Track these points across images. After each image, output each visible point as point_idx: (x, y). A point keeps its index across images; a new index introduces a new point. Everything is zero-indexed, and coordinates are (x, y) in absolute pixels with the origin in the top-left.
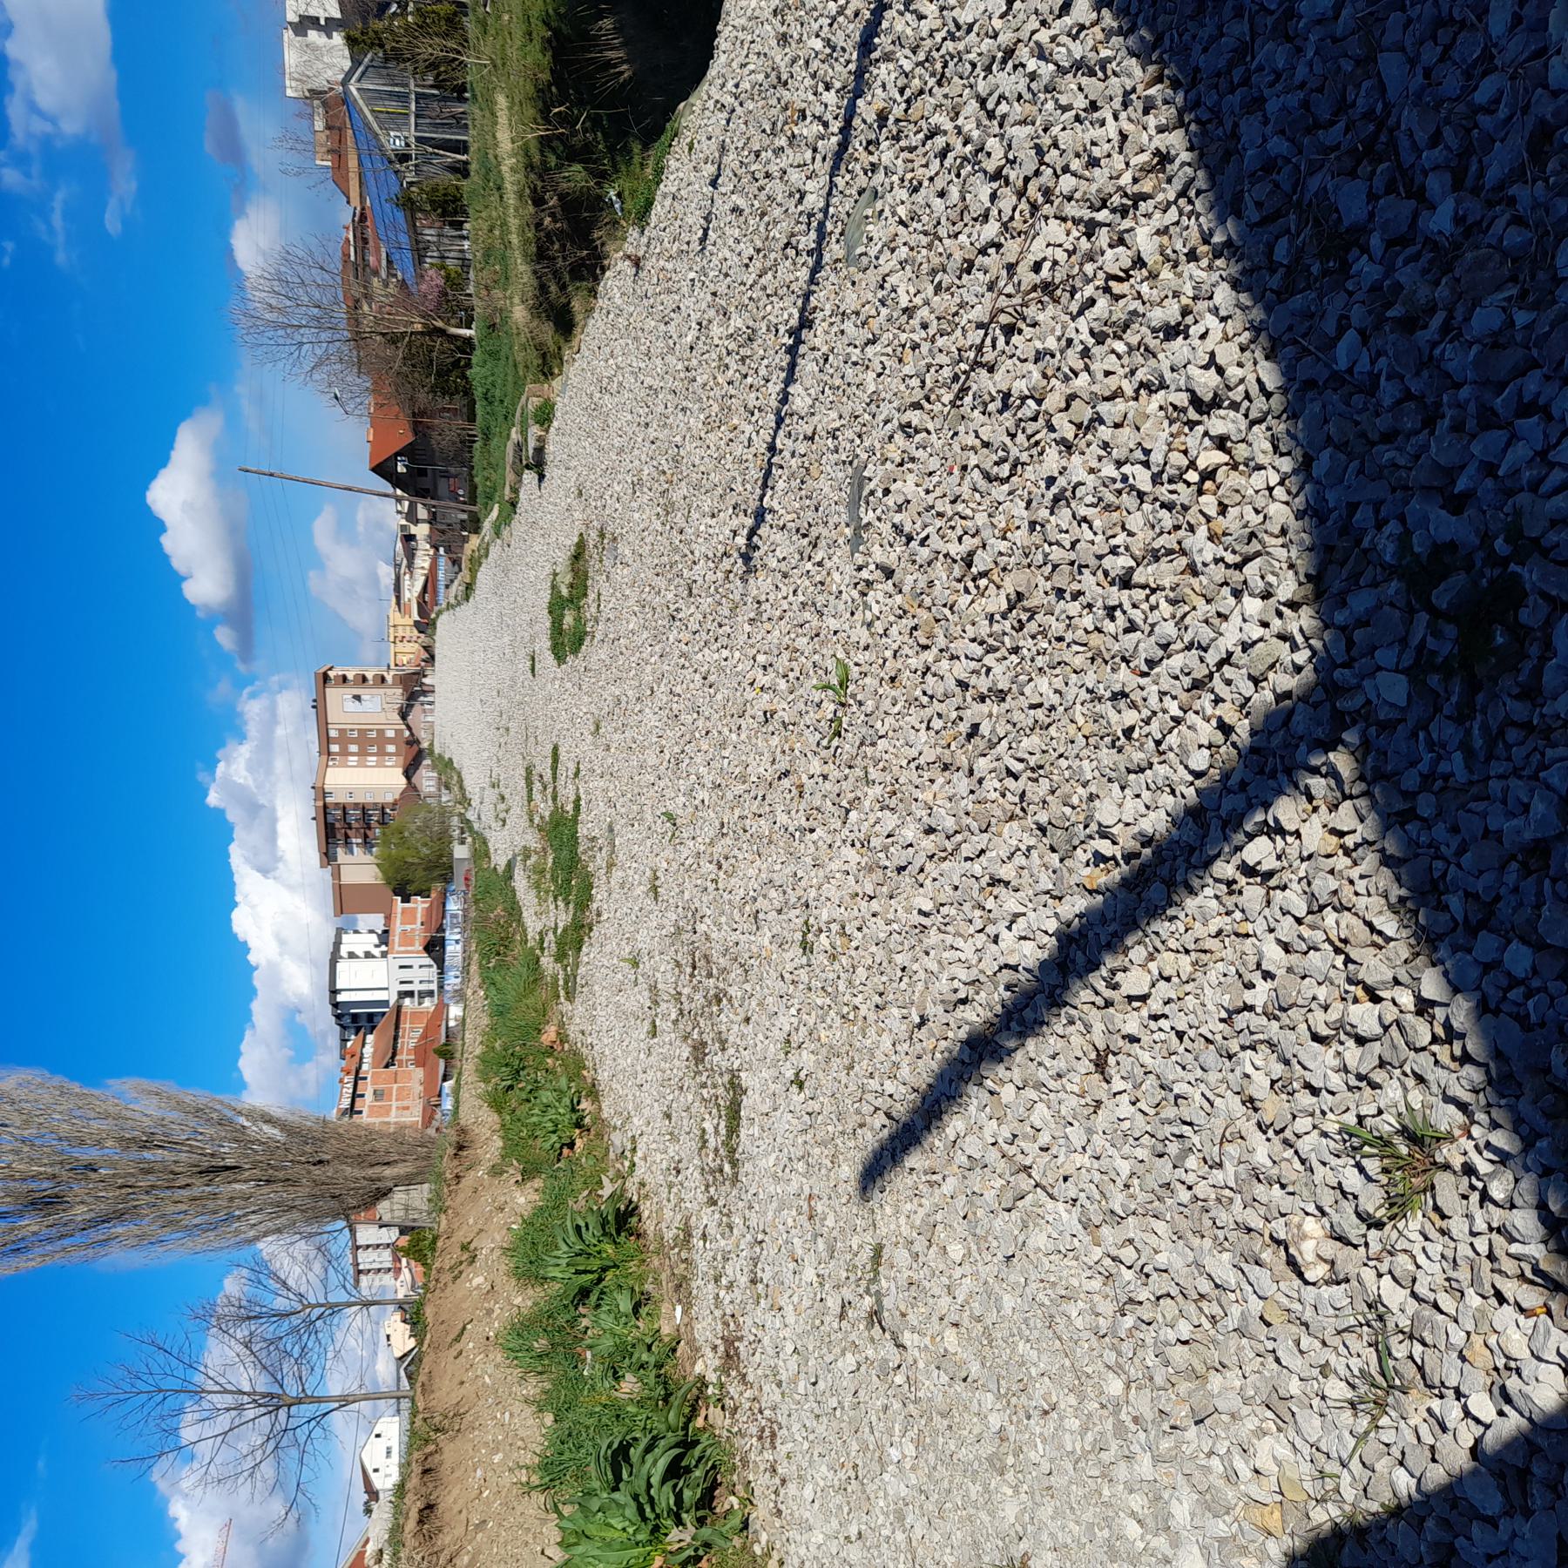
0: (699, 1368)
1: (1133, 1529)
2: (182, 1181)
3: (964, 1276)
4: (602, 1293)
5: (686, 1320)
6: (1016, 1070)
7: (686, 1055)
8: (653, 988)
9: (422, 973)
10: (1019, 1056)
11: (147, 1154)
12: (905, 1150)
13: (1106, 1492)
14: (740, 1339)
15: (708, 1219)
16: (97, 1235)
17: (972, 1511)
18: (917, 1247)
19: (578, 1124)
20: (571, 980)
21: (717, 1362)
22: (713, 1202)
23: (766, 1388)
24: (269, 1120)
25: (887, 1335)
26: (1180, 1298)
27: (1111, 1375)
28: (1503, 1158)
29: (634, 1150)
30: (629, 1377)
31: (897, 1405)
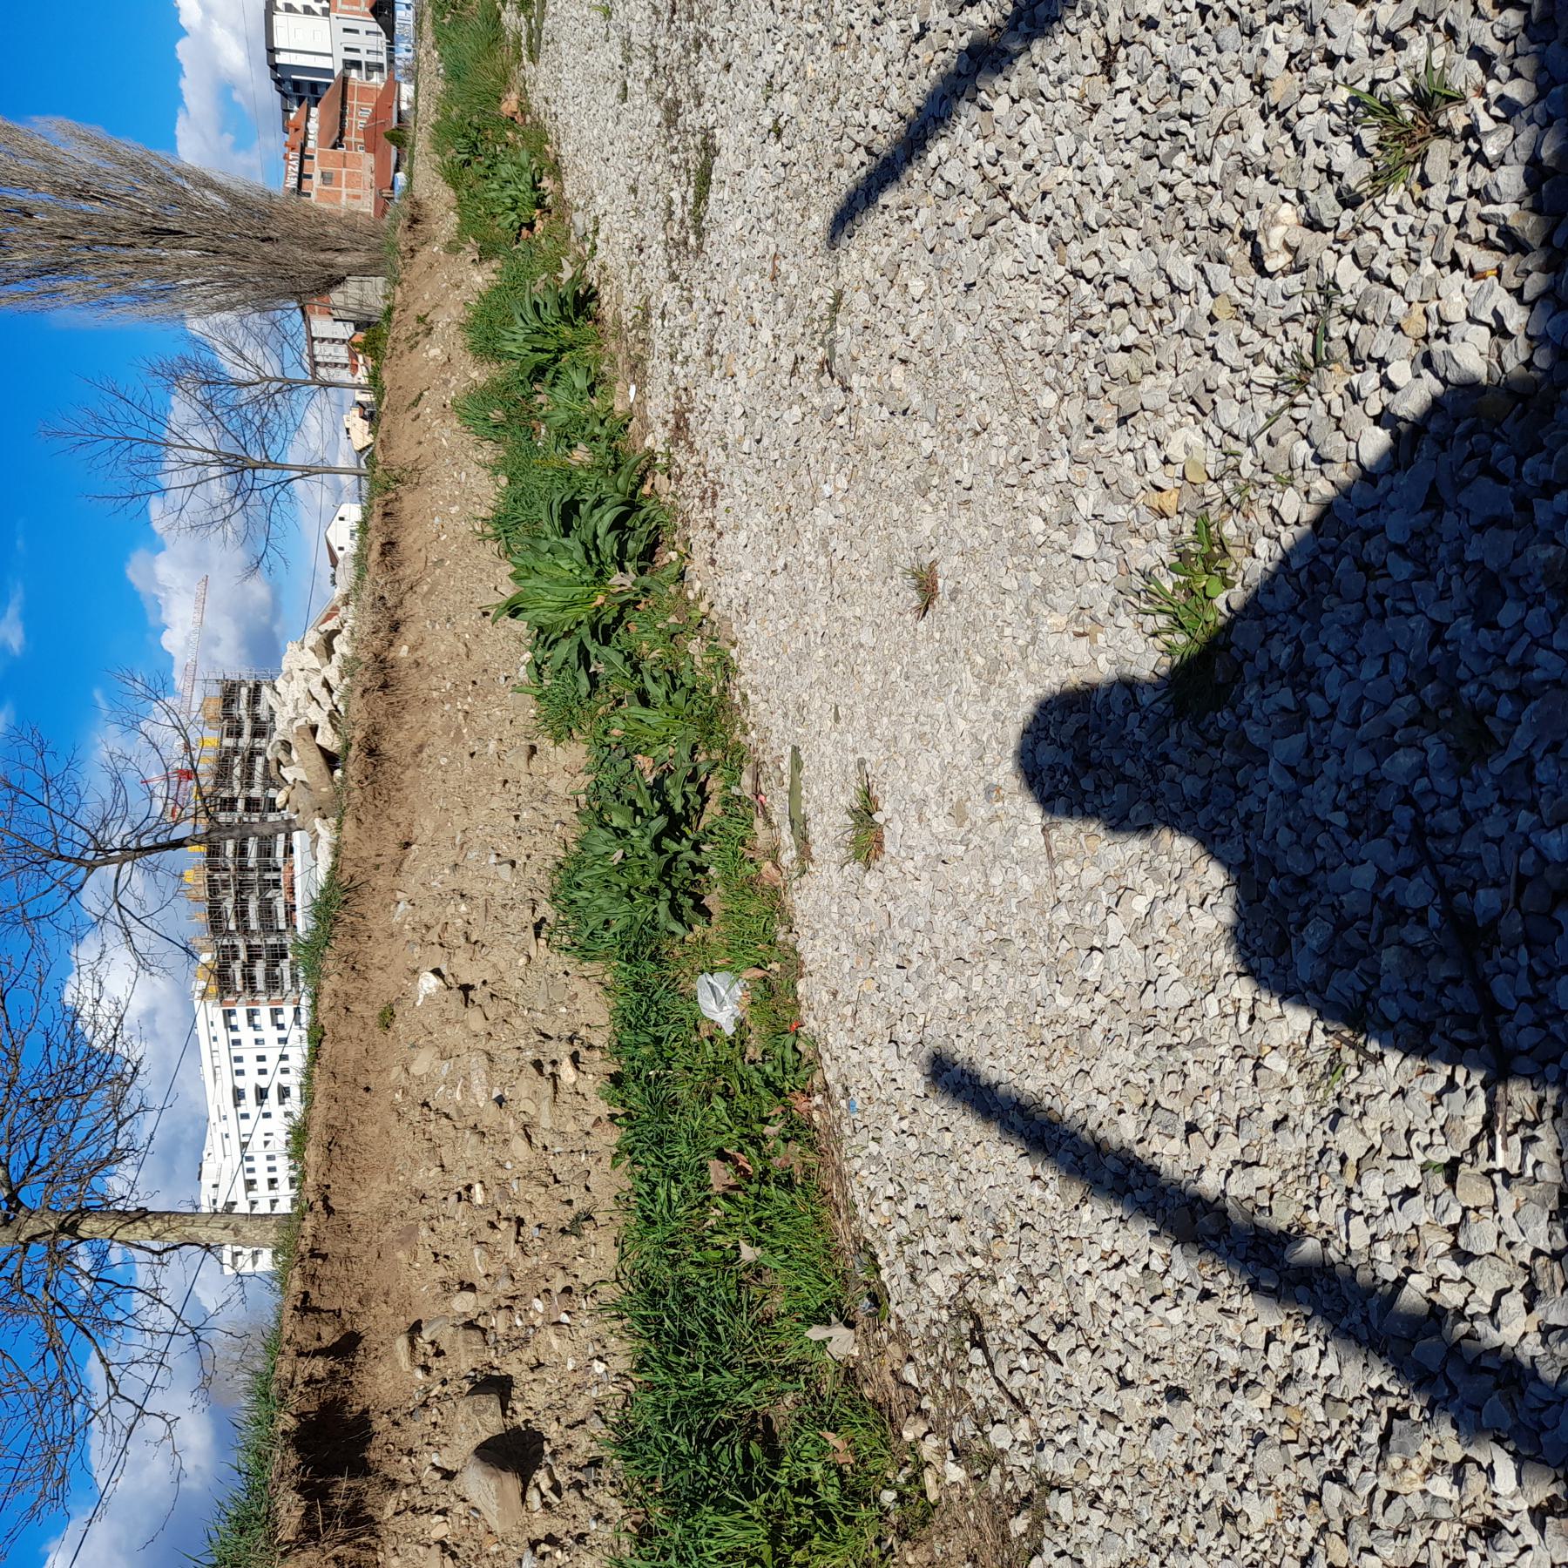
0: (649, 442)
1: (1037, 525)
2: (125, 240)
3: (921, 312)
4: (558, 372)
5: (639, 398)
6: (1015, 79)
7: (657, 119)
8: (627, 44)
9: (370, 43)
10: (1021, 63)
11: (85, 206)
12: (881, 188)
13: (1020, 498)
14: (691, 411)
15: (668, 295)
16: (40, 284)
17: (892, 530)
18: (878, 290)
19: (539, 204)
20: (535, 33)
21: (667, 434)
22: (674, 277)
23: (712, 453)
24: (208, 184)
25: (836, 381)
26: (1133, 307)
27: (1048, 389)
28: (1509, 109)
29: (596, 232)
30: (581, 446)
31: (835, 445)
